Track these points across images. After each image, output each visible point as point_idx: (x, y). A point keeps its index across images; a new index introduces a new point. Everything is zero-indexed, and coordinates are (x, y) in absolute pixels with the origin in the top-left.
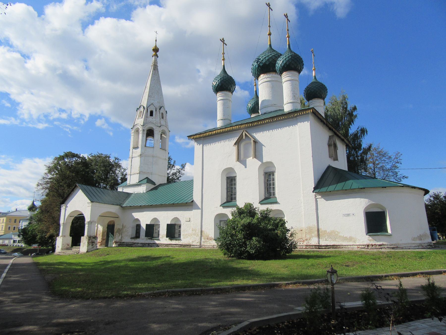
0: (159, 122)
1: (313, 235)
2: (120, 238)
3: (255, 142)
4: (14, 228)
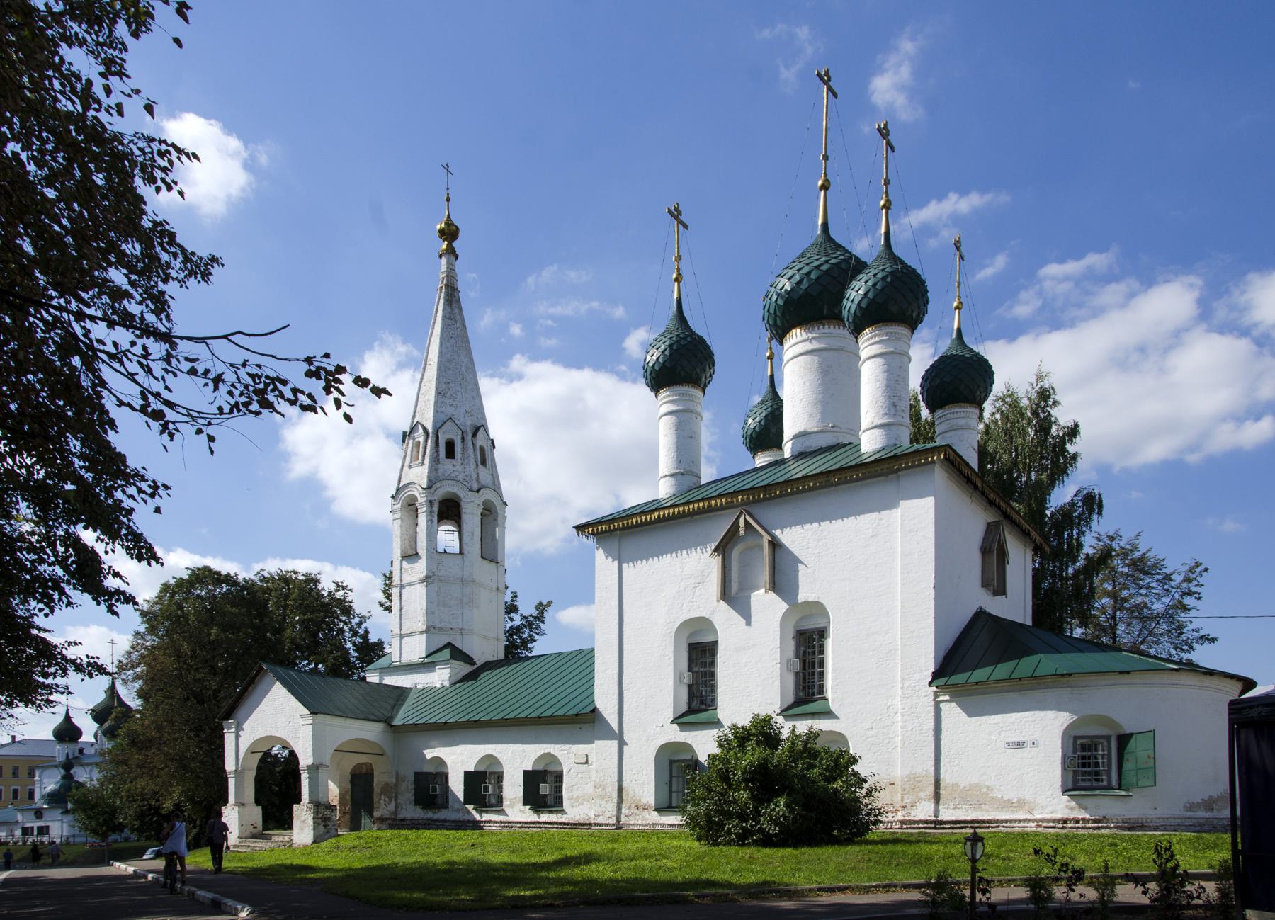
0: (474, 475)
1: (922, 794)
2: (392, 807)
3: (775, 545)
4: (16, 792)
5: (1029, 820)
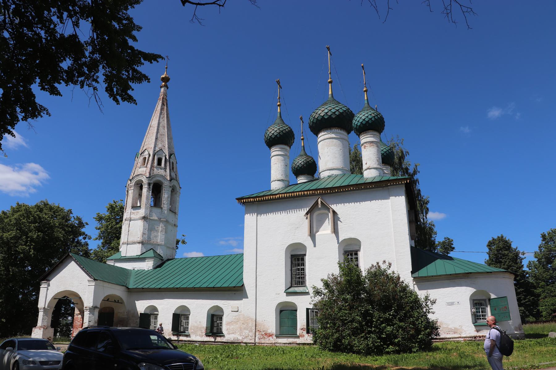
5: (460, 337)
